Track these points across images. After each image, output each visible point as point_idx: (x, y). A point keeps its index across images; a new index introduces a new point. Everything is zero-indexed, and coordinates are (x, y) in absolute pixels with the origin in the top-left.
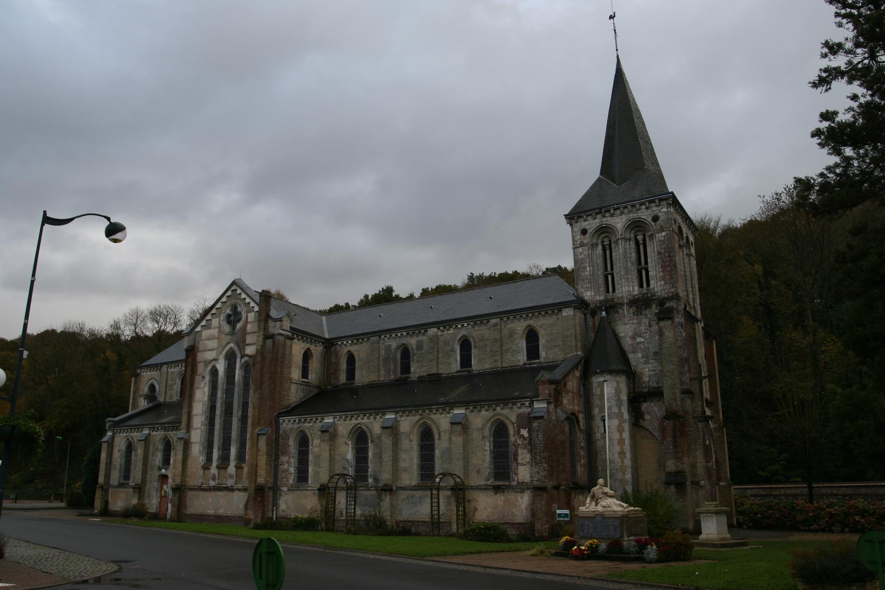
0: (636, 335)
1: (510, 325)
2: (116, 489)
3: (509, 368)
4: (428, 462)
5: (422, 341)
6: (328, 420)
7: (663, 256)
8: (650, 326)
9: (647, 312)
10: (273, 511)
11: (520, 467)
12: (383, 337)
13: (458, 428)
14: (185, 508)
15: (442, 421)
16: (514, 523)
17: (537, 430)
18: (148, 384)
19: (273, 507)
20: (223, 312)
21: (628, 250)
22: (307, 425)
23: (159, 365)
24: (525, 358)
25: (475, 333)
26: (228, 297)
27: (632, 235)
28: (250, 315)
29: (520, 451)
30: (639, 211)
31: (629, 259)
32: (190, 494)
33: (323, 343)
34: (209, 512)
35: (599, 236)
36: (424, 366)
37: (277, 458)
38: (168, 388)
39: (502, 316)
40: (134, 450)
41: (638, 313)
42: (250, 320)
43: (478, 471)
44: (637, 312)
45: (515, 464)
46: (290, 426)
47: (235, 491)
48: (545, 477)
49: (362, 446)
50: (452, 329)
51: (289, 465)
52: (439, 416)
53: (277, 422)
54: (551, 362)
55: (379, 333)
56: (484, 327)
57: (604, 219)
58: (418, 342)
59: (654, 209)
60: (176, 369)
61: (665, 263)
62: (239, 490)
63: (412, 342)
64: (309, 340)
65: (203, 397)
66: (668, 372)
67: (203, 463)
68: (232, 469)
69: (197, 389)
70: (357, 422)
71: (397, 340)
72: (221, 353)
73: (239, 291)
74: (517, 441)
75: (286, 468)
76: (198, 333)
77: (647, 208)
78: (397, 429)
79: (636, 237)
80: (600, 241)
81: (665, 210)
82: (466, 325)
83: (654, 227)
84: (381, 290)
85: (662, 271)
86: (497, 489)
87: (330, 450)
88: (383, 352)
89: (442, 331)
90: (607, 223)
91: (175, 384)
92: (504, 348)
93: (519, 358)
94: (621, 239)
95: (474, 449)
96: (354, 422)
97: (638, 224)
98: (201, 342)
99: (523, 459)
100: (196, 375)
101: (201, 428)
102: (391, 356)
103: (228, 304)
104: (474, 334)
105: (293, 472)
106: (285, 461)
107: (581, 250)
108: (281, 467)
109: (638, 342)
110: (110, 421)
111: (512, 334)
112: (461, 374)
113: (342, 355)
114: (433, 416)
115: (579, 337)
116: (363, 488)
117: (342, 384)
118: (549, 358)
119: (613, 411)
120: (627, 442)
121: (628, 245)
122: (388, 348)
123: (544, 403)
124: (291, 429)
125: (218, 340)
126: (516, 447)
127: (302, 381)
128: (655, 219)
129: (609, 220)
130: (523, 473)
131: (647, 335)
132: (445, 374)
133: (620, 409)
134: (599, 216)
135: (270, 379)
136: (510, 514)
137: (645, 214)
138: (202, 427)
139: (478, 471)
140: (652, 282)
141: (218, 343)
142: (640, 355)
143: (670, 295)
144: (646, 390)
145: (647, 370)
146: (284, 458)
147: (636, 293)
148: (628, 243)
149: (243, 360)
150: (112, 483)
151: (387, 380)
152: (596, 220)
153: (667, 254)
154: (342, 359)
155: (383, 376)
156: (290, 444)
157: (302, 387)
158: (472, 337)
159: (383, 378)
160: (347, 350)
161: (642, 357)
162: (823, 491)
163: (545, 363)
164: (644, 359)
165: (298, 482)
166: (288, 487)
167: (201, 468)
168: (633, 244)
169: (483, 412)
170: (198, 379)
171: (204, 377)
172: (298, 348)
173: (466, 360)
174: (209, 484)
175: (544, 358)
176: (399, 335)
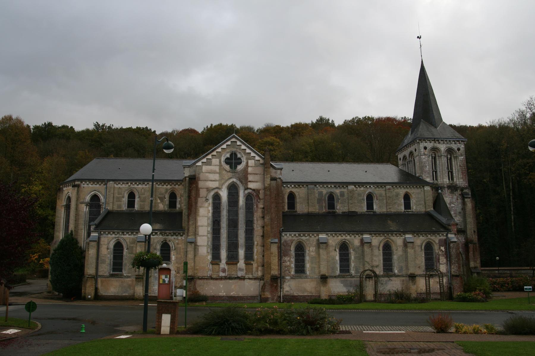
0: (451, 203)
1: (396, 190)
2: (109, 279)
3: (397, 213)
4: (387, 262)
5: (343, 192)
6: (322, 236)
7: (462, 168)
8: (457, 199)
9: (456, 193)
11: (441, 265)
15: (398, 241)
17: (453, 248)
18: (90, 194)
20: (224, 155)
23: (106, 181)
25: (377, 192)
26: (227, 145)
27: (446, 155)
28: (250, 161)
29: (441, 258)
30: (452, 144)
34: (220, 294)
36: (346, 206)
38: (115, 199)
39: (397, 185)
41: (452, 192)
42: (250, 164)
43: (419, 267)
44: (452, 192)
45: (438, 264)
47: (246, 280)
48: (457, 270)
49: (344, 252)
51: (290, 262)
52: (396, 237)
53: (281, 235)
54: (418, 212)
55: (315, 184)
56: (382, 189)
57: (435, 144)
58: (341, 192)
59: (458, 145)
60: (124, 186)
62: (249, 279)
63: (337, 191)
65: (208, 214)
66: (469, 222)
67: (211, 260)
68: (241, 264)
69: (201, 207)
71: (327, 189)
74: (439, 253)
75: (289, 264)
76: (198, 167)
79: (447, 155)
83: (458, 153)
84: (44, 124)
85: (462, 175)
88: (317, 195)
90: (436, 146)
91: (123, 197)
94: (444, 156)
95: (416, 256)
97: (450, 150)
98: (201, 174)
99: (442, 261)
100: (199, 197)
101: (207, 236)
102: (323, 198)
104: (376, 192)
105: (293, 267)
106: (287, 260)
107: (424, 157)
108: (284, 264)
109: (452, 207)
112: (370, 213)
113: (286, 193)
114: (392, 238)
116: (350, 277)
118: (417, 210)
122: (321, 193)
123: (453, 235)
124: (292, 241)
125: (219, 174)
126: (439, 255)
128: (459, 149)
129: (437, 145)
131: (456, 203)
132: (359, 212)
135: (276, 207)
136: (437, 288)
138: (209, 235)
139: (419, 267)
140: (455, 179)
141: (219, 176)
143: (465, 186)
146: (286, 258)
149: (247, 192)
151: (321, 212)
152: (431, 143)
155: (315, 209)
158: (375, 194)
160: (290, 190)
161: (454, 214)
163: (415, 212)
164: (455, 215)
165: (296, 273)
166: (291, 276)
167: (210, 264)
169: (421, 237)
173: (370, 206)
174: (219, 275)
175: (415, 210)
176: (329, 186)
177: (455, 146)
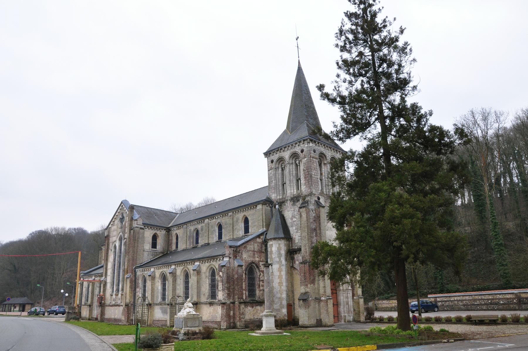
10: (133, 316)
12: (188, 225)
13: (195, 272)
14: (104, 315)
16: (216, 322)
19: (133, 314)
21: (291, 170)
22: (145, 272)
24: (243, 233)
27: (294, 161)
31: (292, 175)
32: (107, 308)
33: (165, 230)
35: (279, 163)
37: (135, 290)
40: (167, 280)
41: (294, 204)
46: (140, 273)
50: (214, 219)
53: (135, 271)
58: (202, 226)
59: (302, 145)
61: (306, 175)
63: (199, 227)
64: (155, 229)
70: (162, 270)
71: (194, 226)
72: (117, 238)
73: (124, 206)
77: (299, 145)
78: (176, 273)
80: (280, 166)
81: (306, 146)
82: (219, 216)
86: (211, 304)
87: (152, 285)
89: (211, 220)
90: (282, 155)
92: (234, 228)
93: (240, 233)
96: (161, 270)
103: (120, 213)
110: (82, 273)
111: (238, 219)
115: (264, 220)
117: (174, 251)
119: (276, 260)
120: (284, 277)
121: (291, 167)
127: (152, 250)
128: (302, 151)
130: (221, 295)
133: (280, 259)
134: (278, 152)
137: (298, 149)
142: (294, 228)
144: (296, 248)
145: (297, 236)
147: (295, 193)
148: (291, 166)
149: (125, 241)
150: (82, 304)
153: (307, 171)
154: (174, 237)
156: (139, 282)
157: (151, 253)
159: (188, 247)
162: (476, 297)
164: (296, 230)
168: (294, 165)
170: (110, 251)
171: (111, 250)
172: (148, 234)
177: (299, 148)
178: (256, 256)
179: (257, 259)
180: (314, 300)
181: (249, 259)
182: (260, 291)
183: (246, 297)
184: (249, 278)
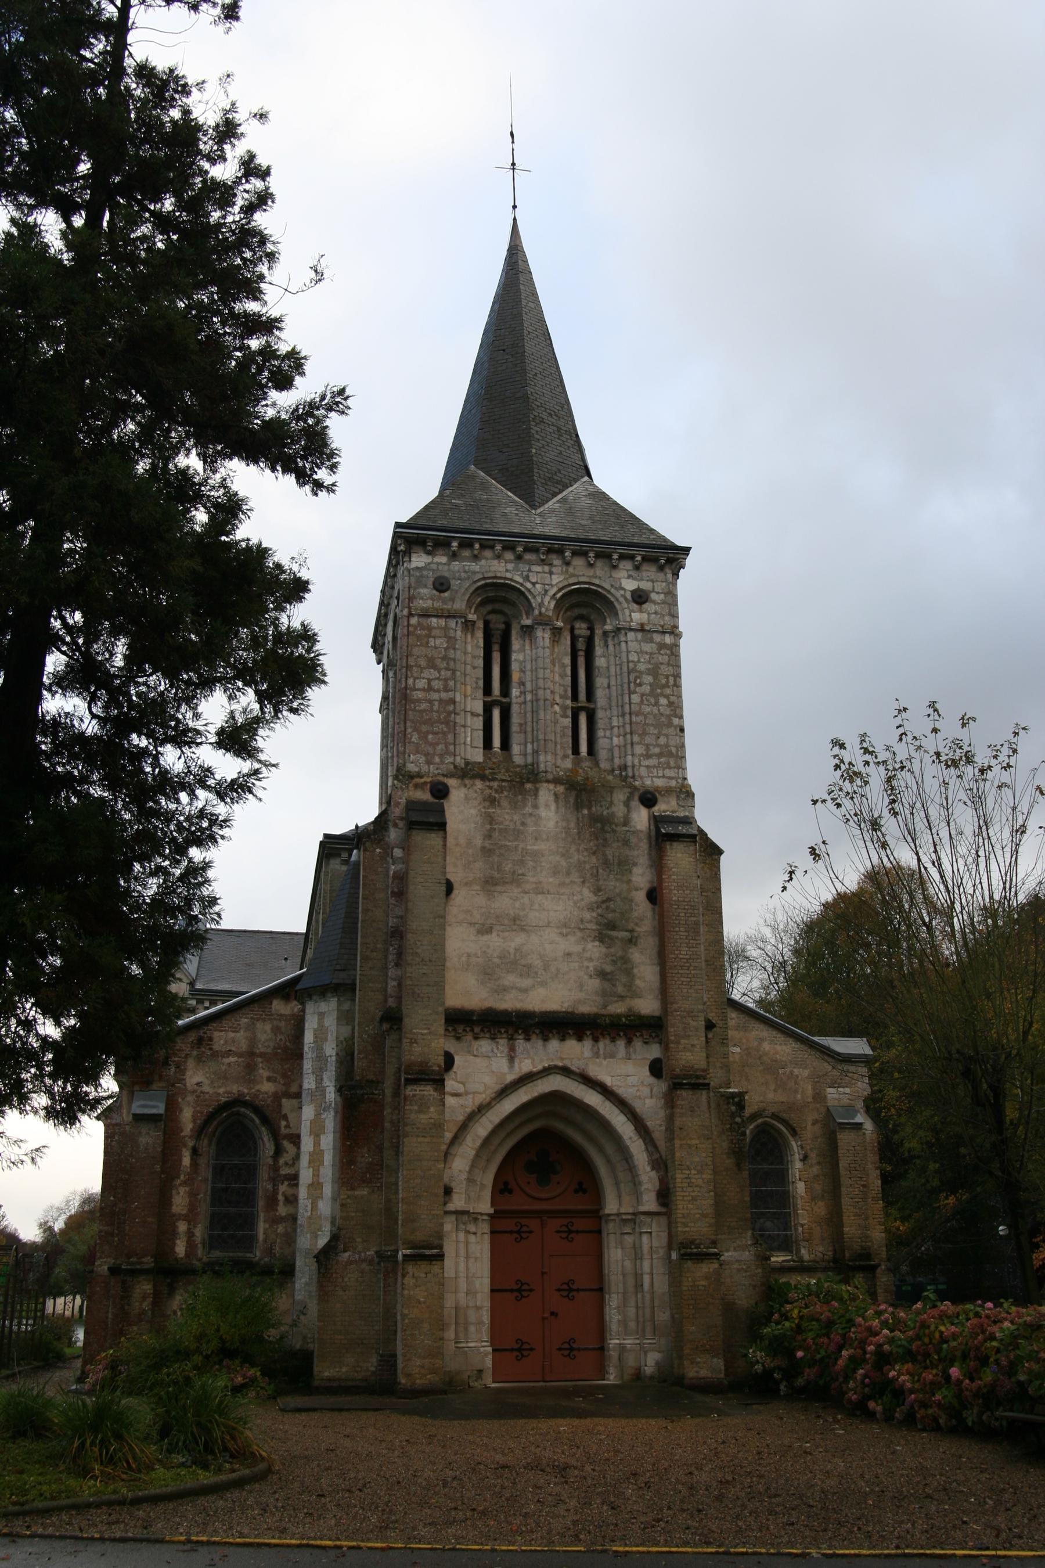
120: (328, 1158)
178: (263, 1072)
179: (268, 1087)
180: (371, 1262)
181: (221, 1090)
182: (275, 1221)
183: (191, 1245)
184: (219, 1171)
